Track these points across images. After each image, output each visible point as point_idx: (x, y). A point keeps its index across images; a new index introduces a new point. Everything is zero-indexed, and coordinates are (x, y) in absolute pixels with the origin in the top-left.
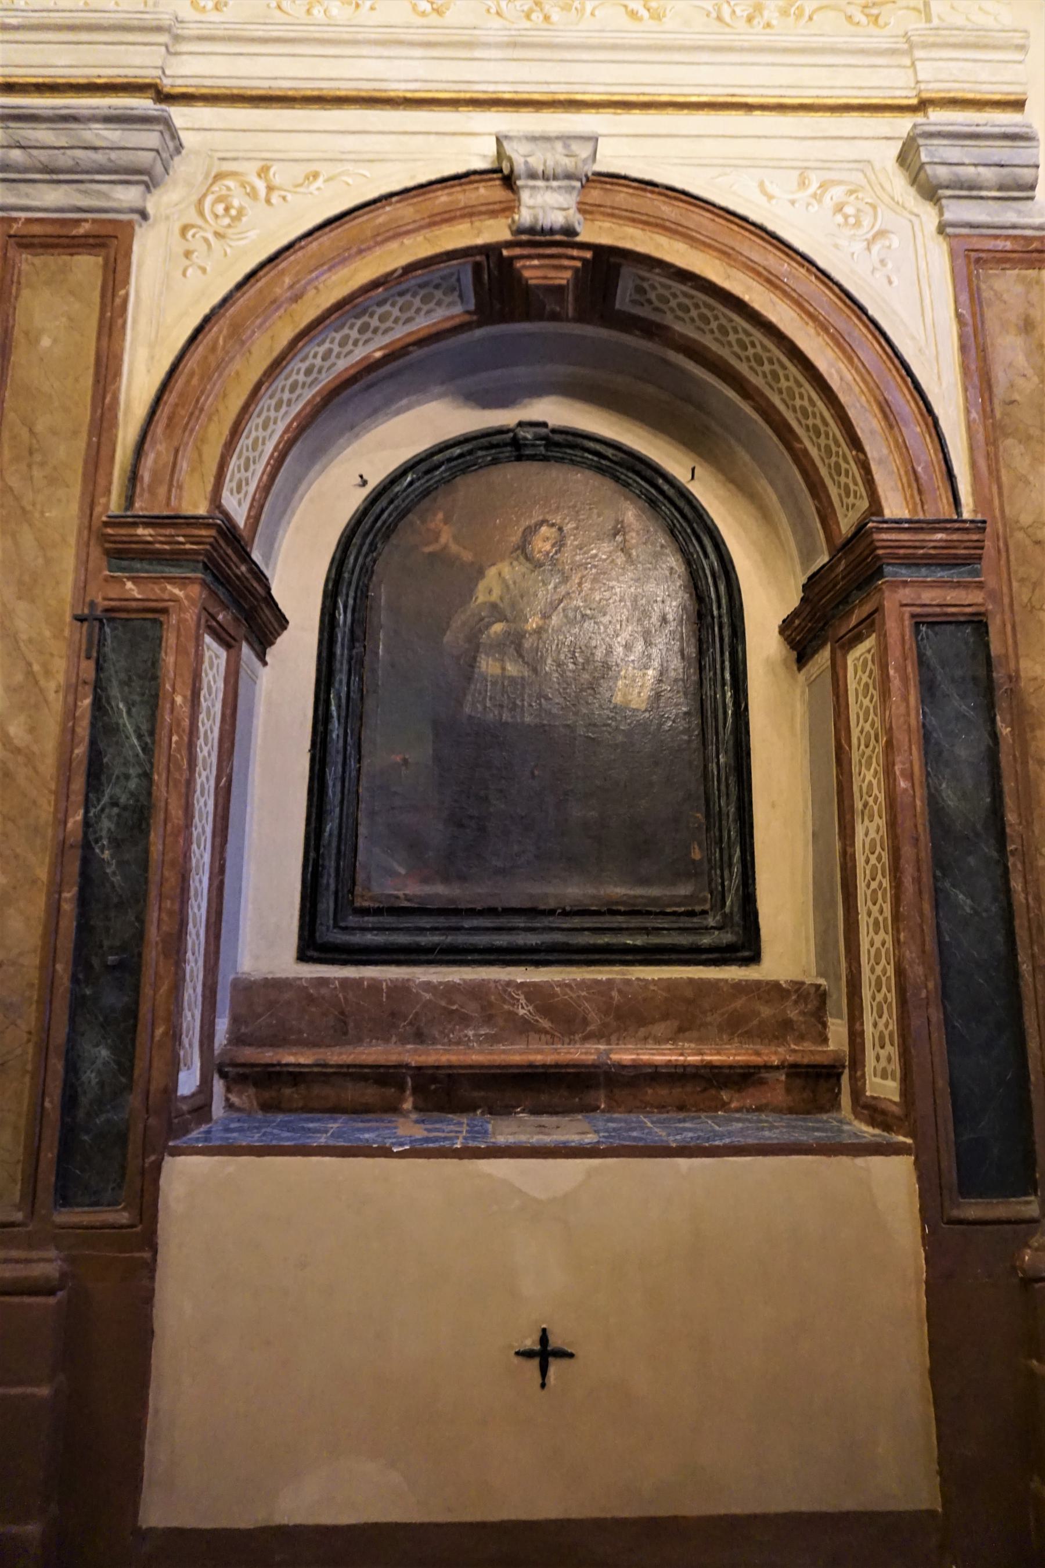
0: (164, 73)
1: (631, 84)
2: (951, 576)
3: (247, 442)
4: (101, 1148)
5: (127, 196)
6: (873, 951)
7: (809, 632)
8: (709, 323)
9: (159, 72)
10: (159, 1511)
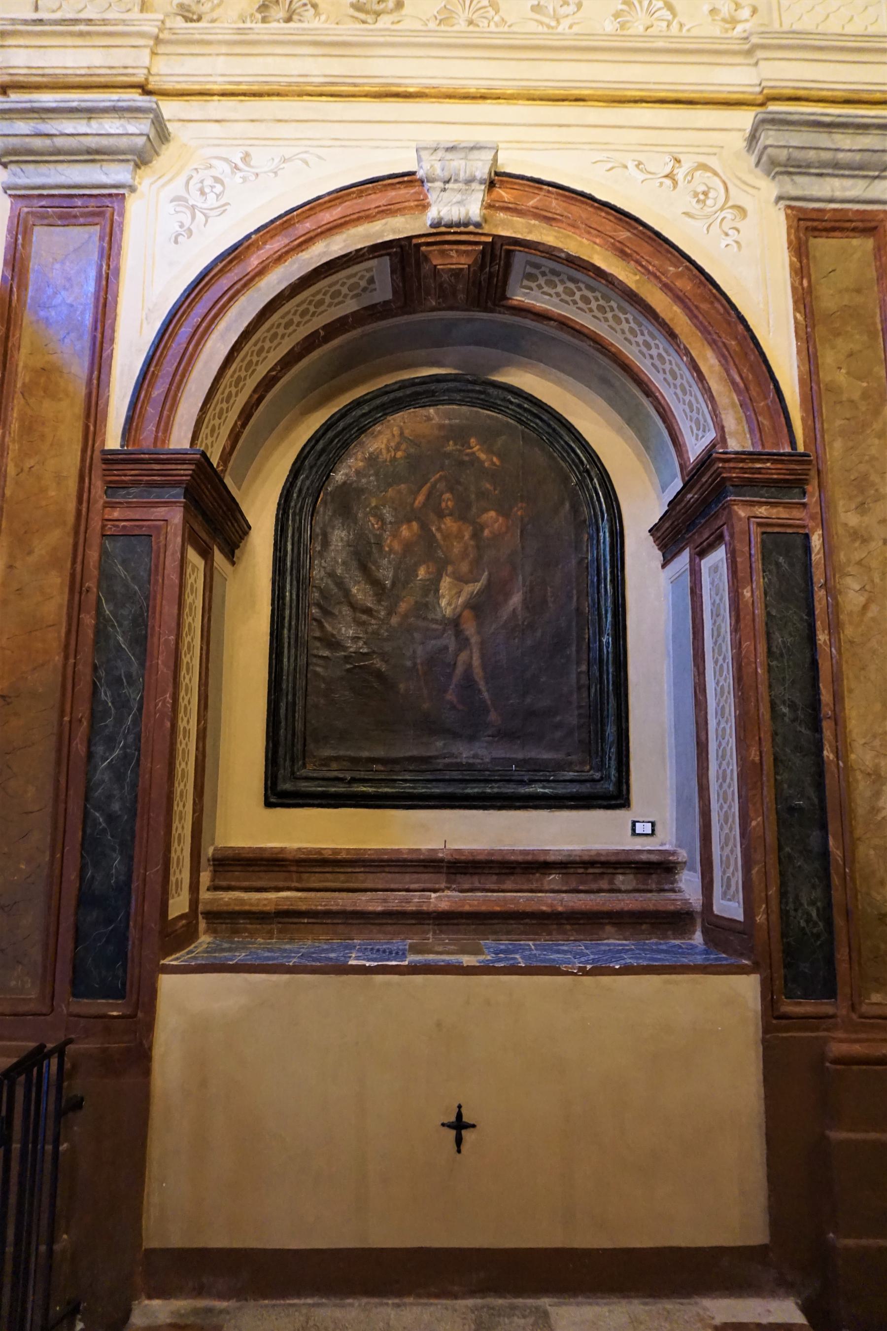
0: (149, 71)
1: (615, 82)
2: (778, 513)
3: (253, 348)
4: (109, 941)
5: (113, 174)
6: (722, 814)
7: (671, 535)
8: (598, 305)
9: (161, 49)
10: (152, 1240)
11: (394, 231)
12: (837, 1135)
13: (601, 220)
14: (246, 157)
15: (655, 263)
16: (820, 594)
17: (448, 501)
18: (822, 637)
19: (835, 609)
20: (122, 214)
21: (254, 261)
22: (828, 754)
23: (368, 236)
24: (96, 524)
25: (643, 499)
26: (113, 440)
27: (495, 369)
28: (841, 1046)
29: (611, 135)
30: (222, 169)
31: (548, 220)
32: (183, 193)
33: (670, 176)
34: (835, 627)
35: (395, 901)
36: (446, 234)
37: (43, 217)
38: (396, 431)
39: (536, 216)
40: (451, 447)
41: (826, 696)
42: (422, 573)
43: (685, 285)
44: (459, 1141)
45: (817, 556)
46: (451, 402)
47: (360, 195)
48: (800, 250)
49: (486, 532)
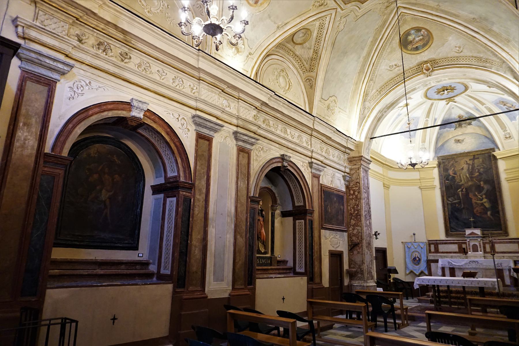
11: (123, 114)
12: (183, 313)
13: (164, 125)
14: (90, 83)
15: (173, 138)
16: (191, 211)
17: (106, 170)
18: (191, 219)
19: (193, 214)
20: (55, 87)
21: (91, 112)
22: (189, 242)
23: (117, 114)
24: (40, 172)
25: (151, 179)
26: (48, 149)
27: (122, 138)
28: (185, 297)
29: (168, 106)
30: (83, 83)
31: (155, 122)
32: (72, 86)
33: (178, 118)
34: (193, 218)
35: (90, 272)
36: (134, 118)
37: (31, 79)
38: (96, 149)
39: (153, 120)
40: (109, 156)
41: (190, 231)
42: (98, 188)
43: (178, 144)
44: (114, 322)
45: (192, 203)
46: (111, 145)
47: (117, 104)
48: (197, 141)
49: (115, 180)
